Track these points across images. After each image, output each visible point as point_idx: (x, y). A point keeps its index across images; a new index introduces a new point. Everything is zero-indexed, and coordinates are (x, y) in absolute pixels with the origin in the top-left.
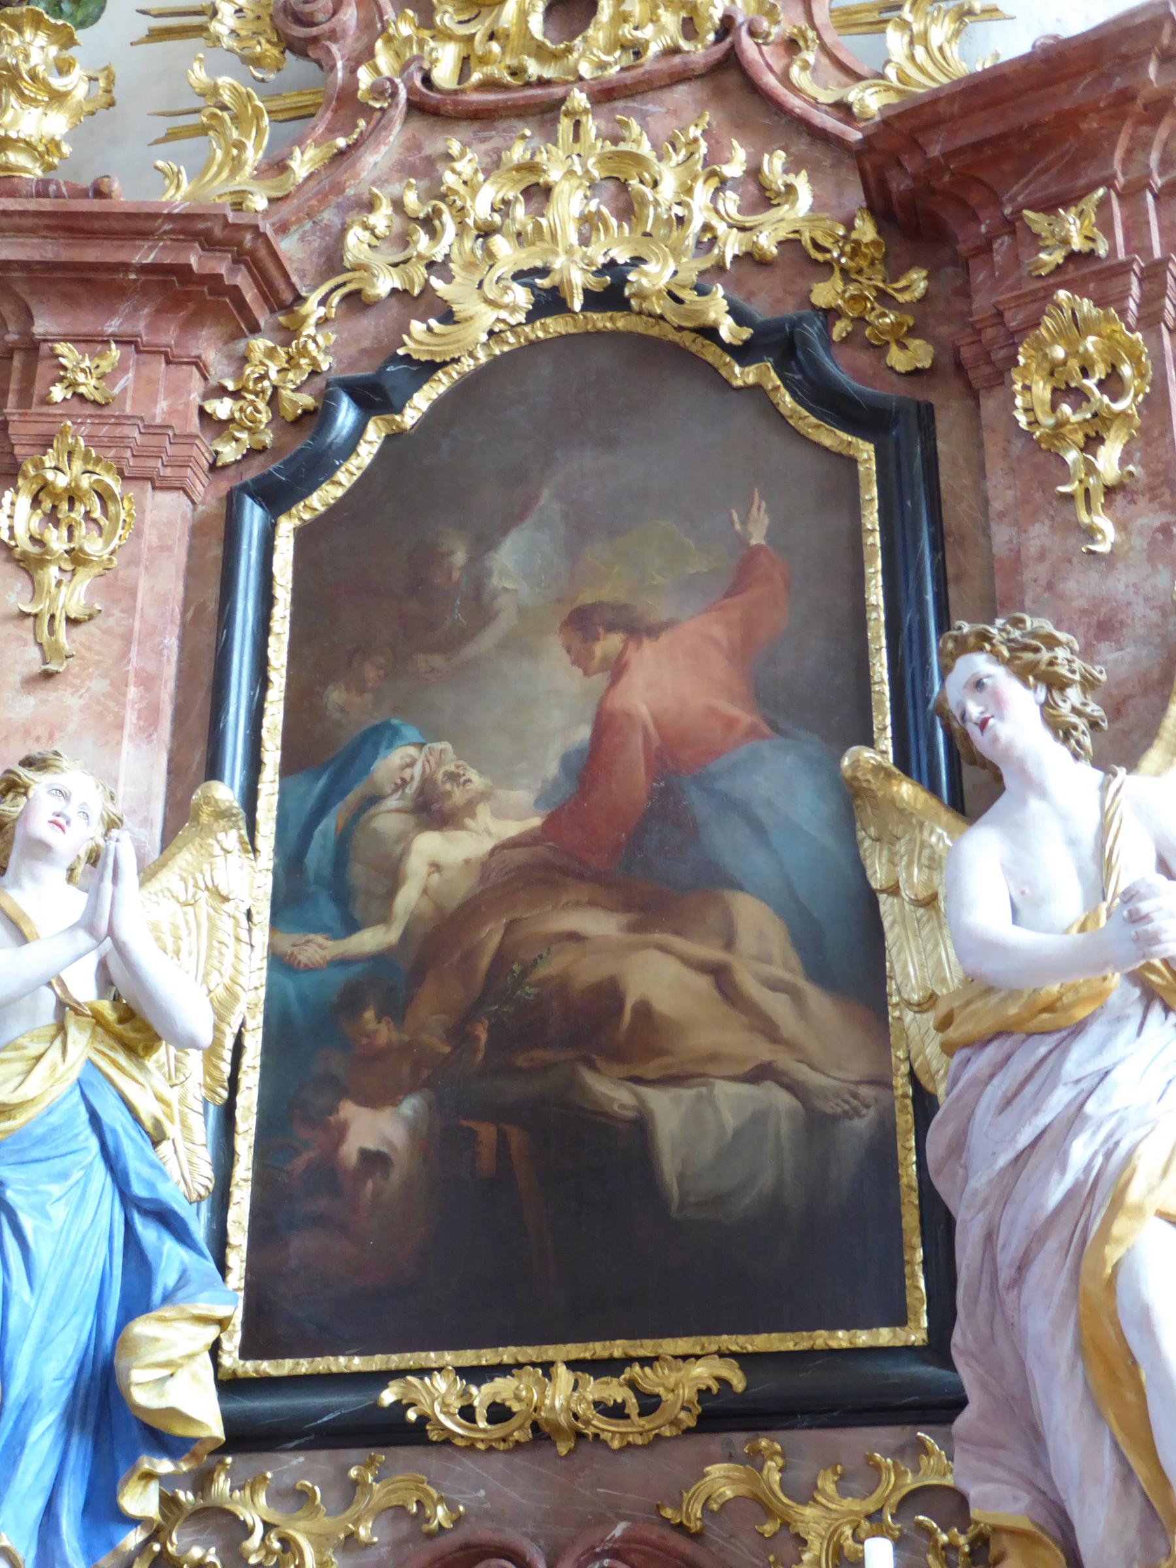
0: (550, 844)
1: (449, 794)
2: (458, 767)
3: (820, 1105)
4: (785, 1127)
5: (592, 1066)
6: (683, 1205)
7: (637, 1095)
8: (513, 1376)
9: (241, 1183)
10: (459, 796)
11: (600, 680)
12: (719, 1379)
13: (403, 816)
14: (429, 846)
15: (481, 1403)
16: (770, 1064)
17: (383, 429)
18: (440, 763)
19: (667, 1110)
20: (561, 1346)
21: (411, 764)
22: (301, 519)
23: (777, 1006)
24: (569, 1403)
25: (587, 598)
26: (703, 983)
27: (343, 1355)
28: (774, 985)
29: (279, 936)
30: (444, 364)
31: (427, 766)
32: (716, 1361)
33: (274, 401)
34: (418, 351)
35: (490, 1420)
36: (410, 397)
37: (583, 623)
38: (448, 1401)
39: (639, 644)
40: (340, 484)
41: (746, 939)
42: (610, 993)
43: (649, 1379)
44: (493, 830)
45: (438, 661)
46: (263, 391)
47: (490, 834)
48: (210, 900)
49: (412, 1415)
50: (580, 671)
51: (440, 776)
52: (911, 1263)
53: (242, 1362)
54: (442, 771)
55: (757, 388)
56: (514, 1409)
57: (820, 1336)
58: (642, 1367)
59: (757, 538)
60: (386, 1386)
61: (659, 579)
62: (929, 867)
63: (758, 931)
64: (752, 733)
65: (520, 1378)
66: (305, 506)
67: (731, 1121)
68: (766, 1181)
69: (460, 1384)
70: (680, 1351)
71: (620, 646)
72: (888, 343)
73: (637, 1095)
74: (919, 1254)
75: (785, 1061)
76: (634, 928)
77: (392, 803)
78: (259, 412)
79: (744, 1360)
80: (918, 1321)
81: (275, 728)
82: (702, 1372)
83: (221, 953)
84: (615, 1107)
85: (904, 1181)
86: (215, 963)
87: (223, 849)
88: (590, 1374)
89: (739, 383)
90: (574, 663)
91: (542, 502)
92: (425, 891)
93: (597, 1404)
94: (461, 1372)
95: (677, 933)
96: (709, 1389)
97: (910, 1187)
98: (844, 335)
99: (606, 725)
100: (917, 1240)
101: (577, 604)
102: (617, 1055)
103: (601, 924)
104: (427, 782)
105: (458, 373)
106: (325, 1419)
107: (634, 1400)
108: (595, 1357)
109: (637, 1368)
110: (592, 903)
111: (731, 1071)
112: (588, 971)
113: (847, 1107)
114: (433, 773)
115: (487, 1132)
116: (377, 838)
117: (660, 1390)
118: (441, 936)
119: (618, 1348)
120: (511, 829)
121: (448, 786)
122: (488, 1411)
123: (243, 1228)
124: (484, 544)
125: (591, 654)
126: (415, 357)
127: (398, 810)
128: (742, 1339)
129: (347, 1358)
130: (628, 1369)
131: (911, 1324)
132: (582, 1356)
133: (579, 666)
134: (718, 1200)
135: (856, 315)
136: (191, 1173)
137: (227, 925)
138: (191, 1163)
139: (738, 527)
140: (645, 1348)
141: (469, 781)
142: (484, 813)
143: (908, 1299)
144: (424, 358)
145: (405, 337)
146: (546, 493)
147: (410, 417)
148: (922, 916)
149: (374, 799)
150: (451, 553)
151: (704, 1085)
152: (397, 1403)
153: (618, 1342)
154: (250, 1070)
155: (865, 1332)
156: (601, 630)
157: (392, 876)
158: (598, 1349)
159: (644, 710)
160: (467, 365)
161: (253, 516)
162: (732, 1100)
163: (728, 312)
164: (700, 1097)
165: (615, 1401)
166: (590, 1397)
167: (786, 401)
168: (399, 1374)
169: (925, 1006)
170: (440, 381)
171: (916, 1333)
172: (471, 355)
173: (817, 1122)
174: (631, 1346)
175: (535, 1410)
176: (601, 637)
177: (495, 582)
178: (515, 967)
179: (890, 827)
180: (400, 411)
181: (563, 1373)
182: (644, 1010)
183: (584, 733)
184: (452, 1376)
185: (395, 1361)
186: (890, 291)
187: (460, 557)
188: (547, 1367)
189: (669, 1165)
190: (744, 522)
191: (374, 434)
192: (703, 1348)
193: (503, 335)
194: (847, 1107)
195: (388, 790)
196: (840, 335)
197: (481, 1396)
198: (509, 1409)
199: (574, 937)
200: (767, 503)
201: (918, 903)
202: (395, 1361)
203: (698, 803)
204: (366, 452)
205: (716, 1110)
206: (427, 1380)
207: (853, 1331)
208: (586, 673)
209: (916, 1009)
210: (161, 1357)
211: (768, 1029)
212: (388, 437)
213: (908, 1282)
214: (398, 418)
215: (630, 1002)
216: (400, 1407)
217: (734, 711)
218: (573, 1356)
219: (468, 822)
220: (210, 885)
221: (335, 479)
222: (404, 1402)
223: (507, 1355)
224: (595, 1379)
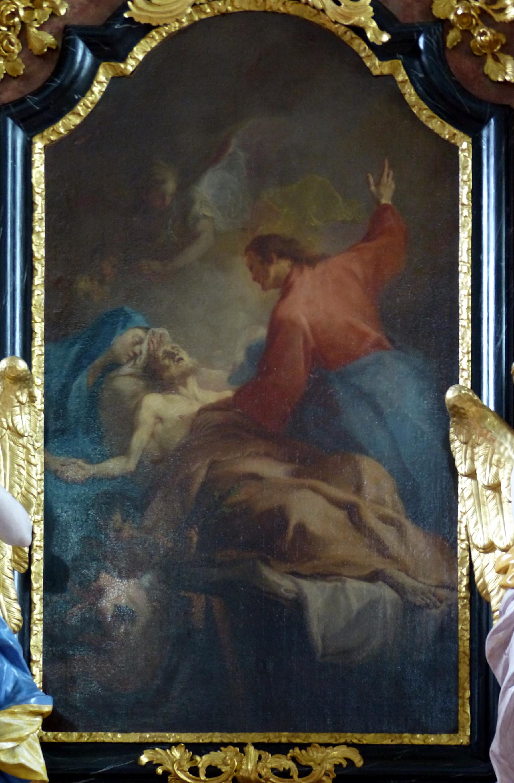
0: (239, 410)
1: (168, 367)
2: (173, 348)
3: (410, 598)
4: (389, 611)
5: (267, 562)
6: (324, 655)
7: (296, 585)
8: (221, 751)
9: (37, 622)
10: (174, 370)
11: (274, 293)
12: (346, 759)
13: (135, 380)
14: (153, 403)
15: (202, 766)
16: (382, 571)
17: (110, 73)
18: (160, 343)
19: (315, 595)
20: (247, 734)
21: (140, 342)
22: (50, 140)
23: (388, 535)
24: (256, 768)
25: (264, 230)
26: (340, 515)
27: (110, 732)
28: (385, 519)
29: (51, 458)
30: (158, 26)
31: (151, 345)
32: (344, 748)
33: (23, 35)
34: (140, 16)
35: (207, 776)
36: (131, 50)
37: (263, 250)
38: (182, 764)
39: (301, 271)
40: (79, 115)
41: (370, 490)
42: (278, 517)
43: (307, 757)
44: (199, 397)
45: (156, 265)
46: (14, 26)
47: (197, 399)
48: (11, 436)
49: (160, 771)
50: (259, 286)
51: (160, 354)
52: (463, 697)
53: (44, 733)
54: (162, 349)
55: (391, 77)
56: (223, 770)
57: (406, 737)
58: (300, 750)
59: (385, 200)
60: (142, 753)
61: (315, 222)
62: (497, 466)
63: (376, 482)
64: (378, 345)
65: (225, 752)
66: (53, 130)
67: (356, 605)
68: (376, 642)
69: (188, 755)
70: (321, 741)
71: (288, 270)
72: (485, 54)
73: (296, 585)
74: (468, 694)
75: (391, 570)
76: (297, 474)
77: (127, 369)
78: (12, 44)
79: (362, 748)
80: (465, 731)
81: (40, 305)
82: (338, 754)
83: (20, 473)
84: (282, 590)
85: (461, 649)
86: (16, 479)
87: (19, 401)
88: (269, 752)
89: (376, 72)
90: (255, 279)
91: (231, 149)
92: (153, 435)
93: (273, 769)
94: (189, 746)
95: (324, 480)
96: (341, 764)
97: (464, 653)
98: (455, 44)
99: (278, 328)
100: (467, 685)
101: (257, 234)
102: (283, 557)
103: (274, 470)
104: (152, 358)
105: (166, 33)
106: (104, 770)
107: (296, 769)
108: (270, 741)
109: (297, 750)
110: (267, 455)
111: (356, 574)
112: (265, 501)
113: (428, 601)
114: (156, 350)
115: (199, 602)
116: (117, 394)
117: (311, 764)
118: (165, 467)
119: (284, 738)
120: (212, 397)
121: (167, 362)
122: (206, 770)
123: (40, 650)
124: (189, 179)
125: (267, 275)
126: (137, 20)
127: (131, 375)
128: (358, 736)
129: (113, 733)
130: (291, 751)
131: (461, 733)
132: (262, 740)
133: (259, 282)
134: (345, 652)
135: (465, 28)
136: (9, 617)
137: (21, 453)
138: (8, 611)
139: (373, 188)
140: (300, 738)
141: (181, 359)
142: (192, 382)
143: (459, 718)
144: (143, 22)
145: (130, 3)
146: (234, 142)
147: (130, 66)
148: (490, 495)
149: (114, 365)
150: (163, 182)
151: (339, 580)
152: (149, 763)
153: (284, 733)
154: (38, 548)
155: (433, 735)
156: (274, 256)
157: (129, 423)
158: (273, 737)
159: (304, 321)
160: (175, 27)
161: (16, 137)
162: (356, 592)
163: (373, 18)
164: (336, 588)
165: (284, 768)
166: (270, 766)
167: (410, 93)
168: (152, 745)
169: (488, 550)
170: (153, 37)
171: (463, 738)
172: (178, 21)
173: (409, 609)
174: (292, 736)
175: (236, 771)
176: (275, 261)
177: (198, 209)
178: (216, 494)
179: (474, 437)
180: (123, 60)
181: (251, 750)
182: (301, 529)
183: (262, 332)
184: (183, 749)
185: (148, 737)
186: (490, 12)
187: (171, 186)
188: (242, 746)
189: (316, 629)
190: (378, 184)
191: (103, 77)
192: (336, 740)
193: (202, 6)
194: (428, 601)
195: (125, 360)
196: (452, 44)
197: (203, 761)
198: (220, 770)
199: (255, 477)
200: (394, 171)
201: (489, 487)
202: (148, 737)
203: (341, 393)
204: (98, 90)
205: (347, 597)
206: (168, 751)
207: (425, 735)
208: (264, 288)
209: (481, 551)
210: (15, 735)
211: (381, 548)
212: (113, 78)
213: (460, 708)
214: (122, 66)
215: (293, 523)
216: (152, 766)
217: (366, 328)
218: (257, 740)
219: (182, 389)
220: (11, 424)
221: (75, 110)
222: (154, 763)
223: (217, 738)
224: (272, 755)
